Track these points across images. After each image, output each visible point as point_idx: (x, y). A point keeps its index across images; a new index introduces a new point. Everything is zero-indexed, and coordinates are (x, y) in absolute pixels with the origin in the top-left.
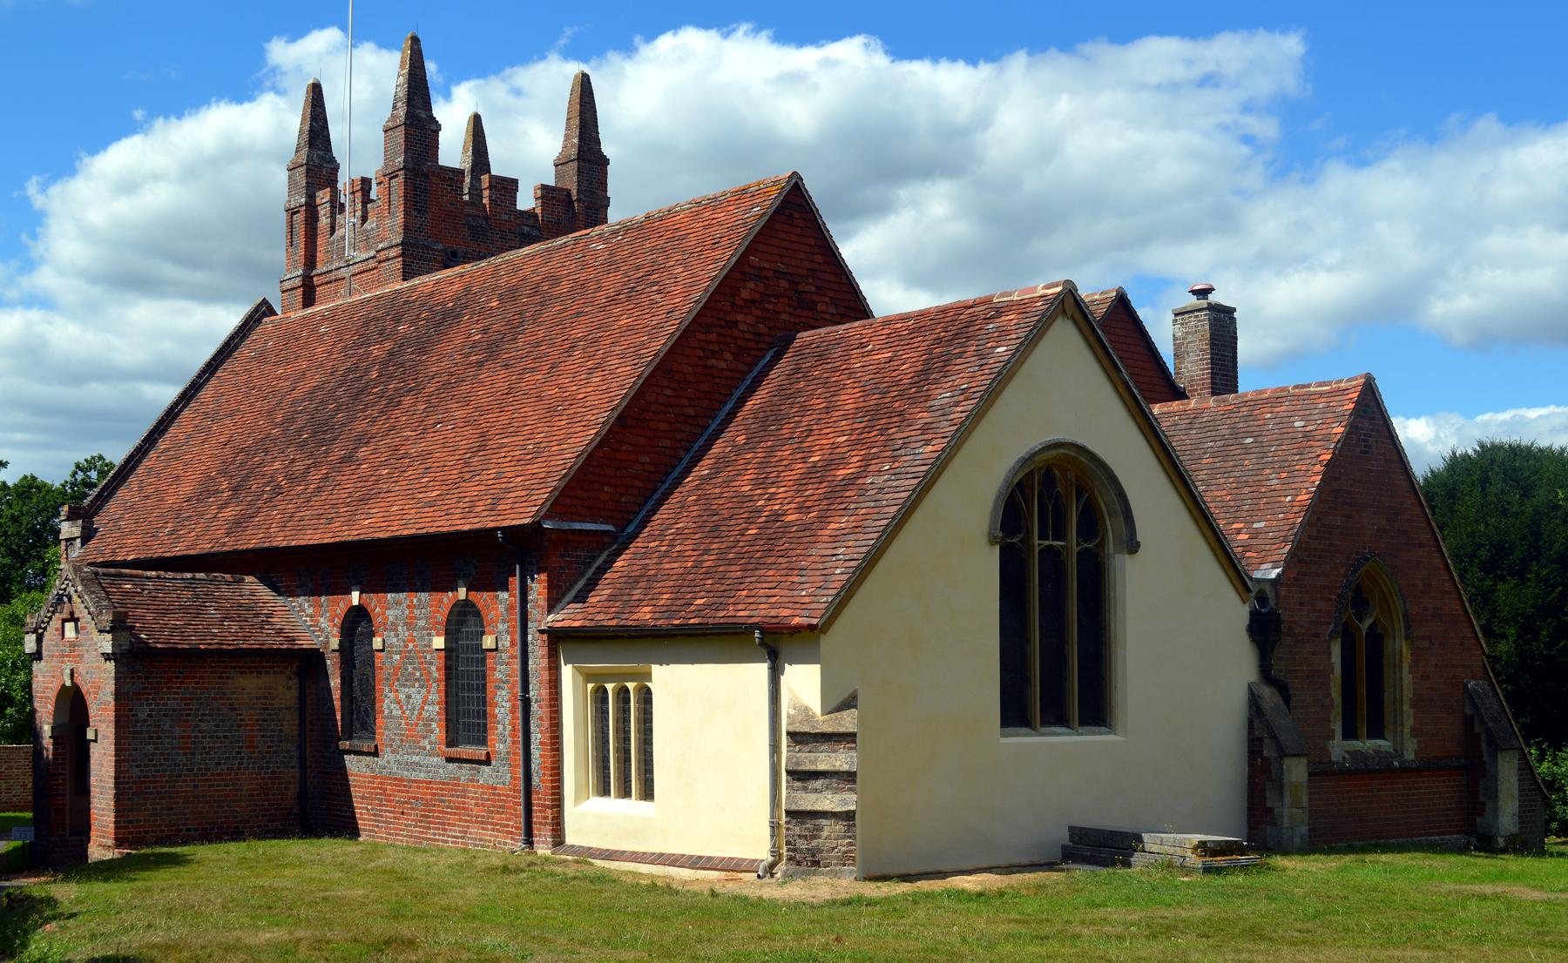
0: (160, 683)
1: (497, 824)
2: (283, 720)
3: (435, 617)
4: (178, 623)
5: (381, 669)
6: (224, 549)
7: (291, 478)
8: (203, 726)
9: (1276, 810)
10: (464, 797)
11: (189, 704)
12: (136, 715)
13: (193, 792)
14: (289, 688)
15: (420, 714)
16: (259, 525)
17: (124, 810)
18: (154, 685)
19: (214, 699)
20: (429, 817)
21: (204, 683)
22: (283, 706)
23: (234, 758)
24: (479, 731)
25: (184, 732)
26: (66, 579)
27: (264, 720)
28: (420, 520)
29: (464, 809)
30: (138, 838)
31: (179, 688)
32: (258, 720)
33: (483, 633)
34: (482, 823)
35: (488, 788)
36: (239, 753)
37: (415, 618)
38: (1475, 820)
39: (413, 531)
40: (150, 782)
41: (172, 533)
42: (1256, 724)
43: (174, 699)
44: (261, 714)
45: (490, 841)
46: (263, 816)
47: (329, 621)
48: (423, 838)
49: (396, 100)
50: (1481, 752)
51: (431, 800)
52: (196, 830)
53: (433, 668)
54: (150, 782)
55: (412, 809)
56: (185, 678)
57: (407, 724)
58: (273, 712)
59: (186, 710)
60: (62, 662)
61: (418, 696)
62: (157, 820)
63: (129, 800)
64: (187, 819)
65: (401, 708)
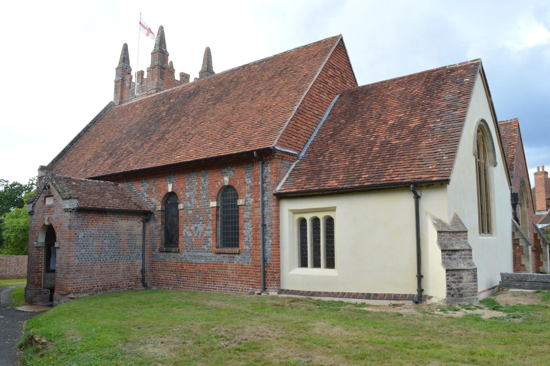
0: (88, 222)
1: (244, 281)
2: (136, 239)
3: (211, 194)
4: (96, 198)
5: (182, 217)
6: (109, 173)
7: (136, 148)
8: (105, 241)
9: (526, 265)
10: (226, 269)
11: (100, 232)
12: (78, 236)
13: (100, 270)
14: (139, 227)
15: (202, 235)
16: (124, 164)
17: (71, 278)
18: (86, 223)
19: (110, 230)
20: (206, 278)
21: (106, 223)
22: (137, 234)
23: (117, 255)
24: (235, 241)
25: (98, 244)
26: (48, 179)
27: (129, 240)
28: (207, 153)
29: (226, 275)
30: (77, 290)
31: (97, 225)
32: (127, 239)
33: (238, 199)
34: (235, 280)
35: (239, 265)
36: (119, 253)
37: (201, 195)
38: (539, 268)
39: (205, 157)
40: (83, 266)
41: (84, 171)
42: (516, 234)
43: (94, 230)
44: (128, 237)
45: (240, 289)
46: (128, 279)
47: (156, 199)
48: (203, 288)
49: (155, 45)
50: (541, 245)
51: (207, 271)
52: (101, 286)
53: (210, 215)
54: (83, 266)
55: (197, 275)
56: (99, 221)
57: (195, 239)
58: (133, 236)
59: (99, 234)
60: (44, 215)
61: (201, 228)
62: (85, 283)
63: (74, 274)
64: (98, 281)
65: (192, 233)
